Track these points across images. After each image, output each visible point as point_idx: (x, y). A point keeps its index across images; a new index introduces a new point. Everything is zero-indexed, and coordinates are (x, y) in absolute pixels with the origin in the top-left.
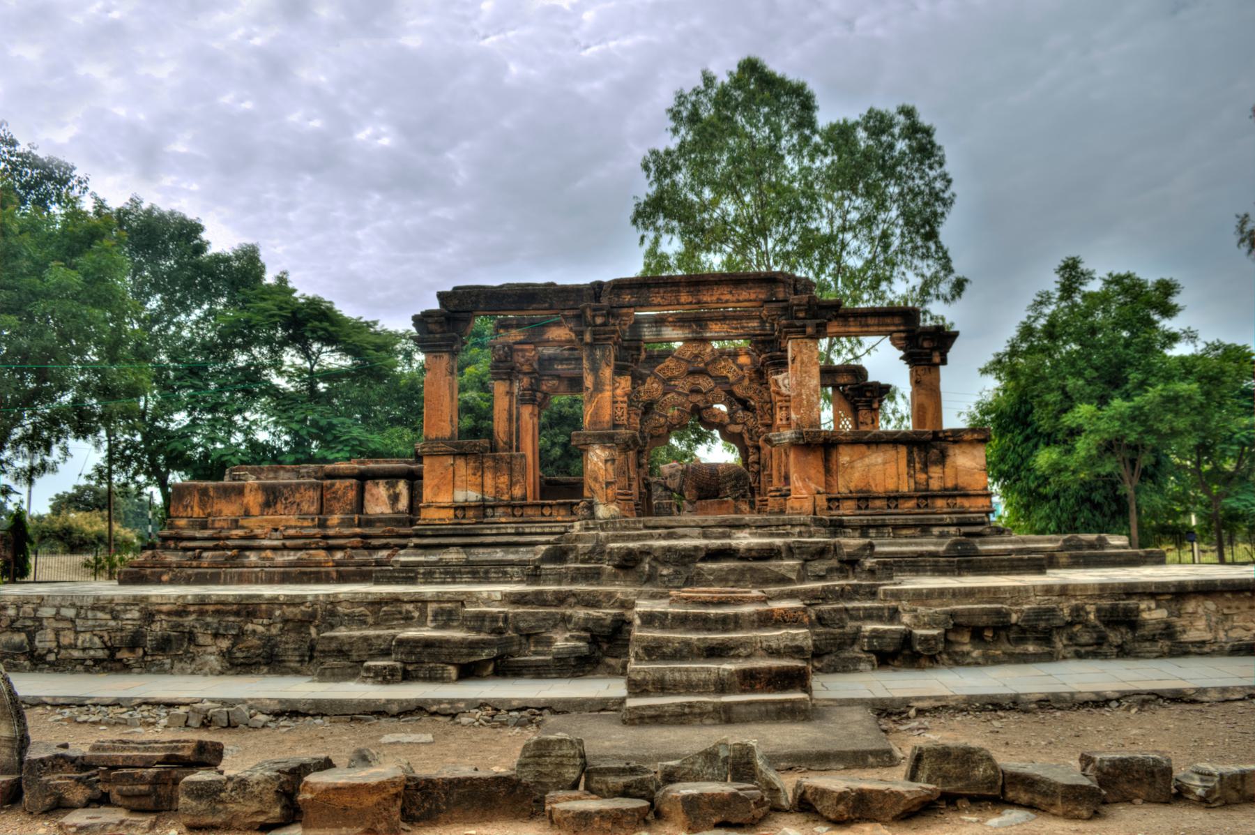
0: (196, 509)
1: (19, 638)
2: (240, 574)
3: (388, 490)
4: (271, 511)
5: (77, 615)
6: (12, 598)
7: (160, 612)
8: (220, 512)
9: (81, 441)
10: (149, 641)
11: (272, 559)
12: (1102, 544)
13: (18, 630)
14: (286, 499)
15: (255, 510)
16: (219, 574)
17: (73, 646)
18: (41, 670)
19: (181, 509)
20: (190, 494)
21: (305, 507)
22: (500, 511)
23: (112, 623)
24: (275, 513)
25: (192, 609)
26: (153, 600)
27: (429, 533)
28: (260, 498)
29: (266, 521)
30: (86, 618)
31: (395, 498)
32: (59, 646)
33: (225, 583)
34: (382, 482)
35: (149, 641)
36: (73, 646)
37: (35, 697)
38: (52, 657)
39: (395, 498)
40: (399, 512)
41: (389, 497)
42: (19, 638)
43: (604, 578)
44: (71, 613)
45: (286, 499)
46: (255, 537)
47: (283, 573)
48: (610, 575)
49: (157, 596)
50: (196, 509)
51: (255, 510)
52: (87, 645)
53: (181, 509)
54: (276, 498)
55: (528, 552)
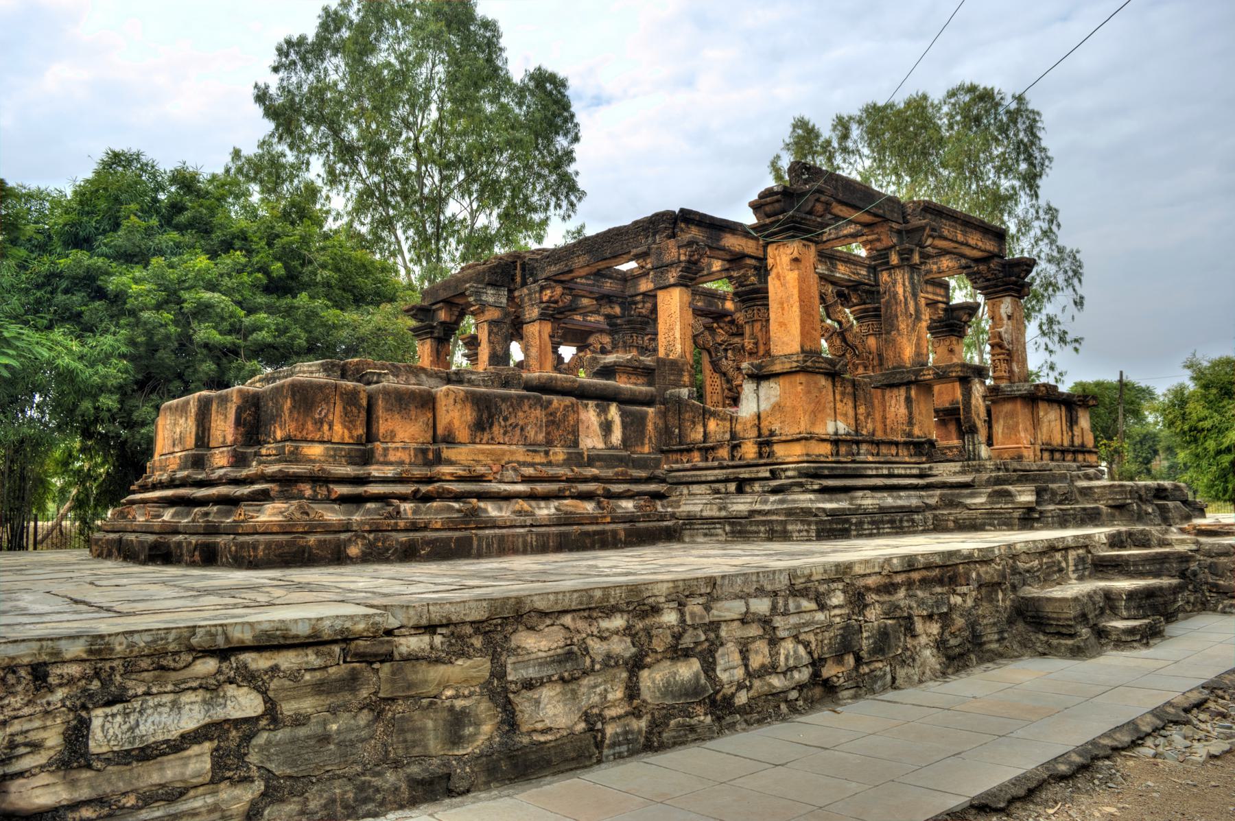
0: (338, 428)
1: (688, 670)
2: (502, 538)
3: (599, 415)
4: (486, 437)
5: (774, 608)
6: (664, 588)
7: (868, 589)
8: (393, 435)
9: (989, 87)
10: (865, 643)
11: (532, 514)
12: (396, 524)
13: (687, 654)
14: (506, 419)
15: (462, 434)
16: (470, 539)
17: (772, 669)
18: (732, 726)
19: (310, 426)
20: (326, 399)
21: (531, 433)
22: (864, 448)
23: (820, 616)
24: (491, 441)
25: (899, 579)
26: (858, 570)
27: (826, 472)
28: (469, 415)
29: (483, 452)
30: (786, 613)
31: (607, 428)
32: (749, 674)
33: (479, 556)
34: (591, 403)
35: (865, 643)
36: (772, 669)
37: (1017, 781)
38: (742, 698)
39: (607, 428)
40: (613, 448)
41: (601, 425)
42: (688, 670)
43: (1104, 517)
44: (761, 606)
45: (506, 419)
46: (479, 479)
47: (561, 535)
48: (1107, 514)
49: (861, 562)
50: (338, 428)
51: (462, 434)
52: (791, 662)
53: (310, 426)
54: (491, 416)
55: (909, 497)
